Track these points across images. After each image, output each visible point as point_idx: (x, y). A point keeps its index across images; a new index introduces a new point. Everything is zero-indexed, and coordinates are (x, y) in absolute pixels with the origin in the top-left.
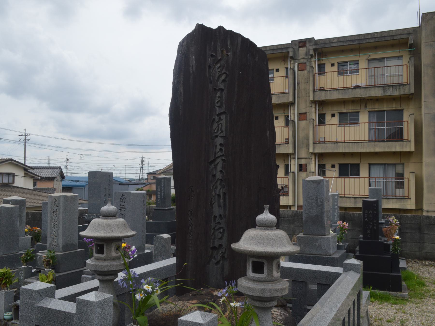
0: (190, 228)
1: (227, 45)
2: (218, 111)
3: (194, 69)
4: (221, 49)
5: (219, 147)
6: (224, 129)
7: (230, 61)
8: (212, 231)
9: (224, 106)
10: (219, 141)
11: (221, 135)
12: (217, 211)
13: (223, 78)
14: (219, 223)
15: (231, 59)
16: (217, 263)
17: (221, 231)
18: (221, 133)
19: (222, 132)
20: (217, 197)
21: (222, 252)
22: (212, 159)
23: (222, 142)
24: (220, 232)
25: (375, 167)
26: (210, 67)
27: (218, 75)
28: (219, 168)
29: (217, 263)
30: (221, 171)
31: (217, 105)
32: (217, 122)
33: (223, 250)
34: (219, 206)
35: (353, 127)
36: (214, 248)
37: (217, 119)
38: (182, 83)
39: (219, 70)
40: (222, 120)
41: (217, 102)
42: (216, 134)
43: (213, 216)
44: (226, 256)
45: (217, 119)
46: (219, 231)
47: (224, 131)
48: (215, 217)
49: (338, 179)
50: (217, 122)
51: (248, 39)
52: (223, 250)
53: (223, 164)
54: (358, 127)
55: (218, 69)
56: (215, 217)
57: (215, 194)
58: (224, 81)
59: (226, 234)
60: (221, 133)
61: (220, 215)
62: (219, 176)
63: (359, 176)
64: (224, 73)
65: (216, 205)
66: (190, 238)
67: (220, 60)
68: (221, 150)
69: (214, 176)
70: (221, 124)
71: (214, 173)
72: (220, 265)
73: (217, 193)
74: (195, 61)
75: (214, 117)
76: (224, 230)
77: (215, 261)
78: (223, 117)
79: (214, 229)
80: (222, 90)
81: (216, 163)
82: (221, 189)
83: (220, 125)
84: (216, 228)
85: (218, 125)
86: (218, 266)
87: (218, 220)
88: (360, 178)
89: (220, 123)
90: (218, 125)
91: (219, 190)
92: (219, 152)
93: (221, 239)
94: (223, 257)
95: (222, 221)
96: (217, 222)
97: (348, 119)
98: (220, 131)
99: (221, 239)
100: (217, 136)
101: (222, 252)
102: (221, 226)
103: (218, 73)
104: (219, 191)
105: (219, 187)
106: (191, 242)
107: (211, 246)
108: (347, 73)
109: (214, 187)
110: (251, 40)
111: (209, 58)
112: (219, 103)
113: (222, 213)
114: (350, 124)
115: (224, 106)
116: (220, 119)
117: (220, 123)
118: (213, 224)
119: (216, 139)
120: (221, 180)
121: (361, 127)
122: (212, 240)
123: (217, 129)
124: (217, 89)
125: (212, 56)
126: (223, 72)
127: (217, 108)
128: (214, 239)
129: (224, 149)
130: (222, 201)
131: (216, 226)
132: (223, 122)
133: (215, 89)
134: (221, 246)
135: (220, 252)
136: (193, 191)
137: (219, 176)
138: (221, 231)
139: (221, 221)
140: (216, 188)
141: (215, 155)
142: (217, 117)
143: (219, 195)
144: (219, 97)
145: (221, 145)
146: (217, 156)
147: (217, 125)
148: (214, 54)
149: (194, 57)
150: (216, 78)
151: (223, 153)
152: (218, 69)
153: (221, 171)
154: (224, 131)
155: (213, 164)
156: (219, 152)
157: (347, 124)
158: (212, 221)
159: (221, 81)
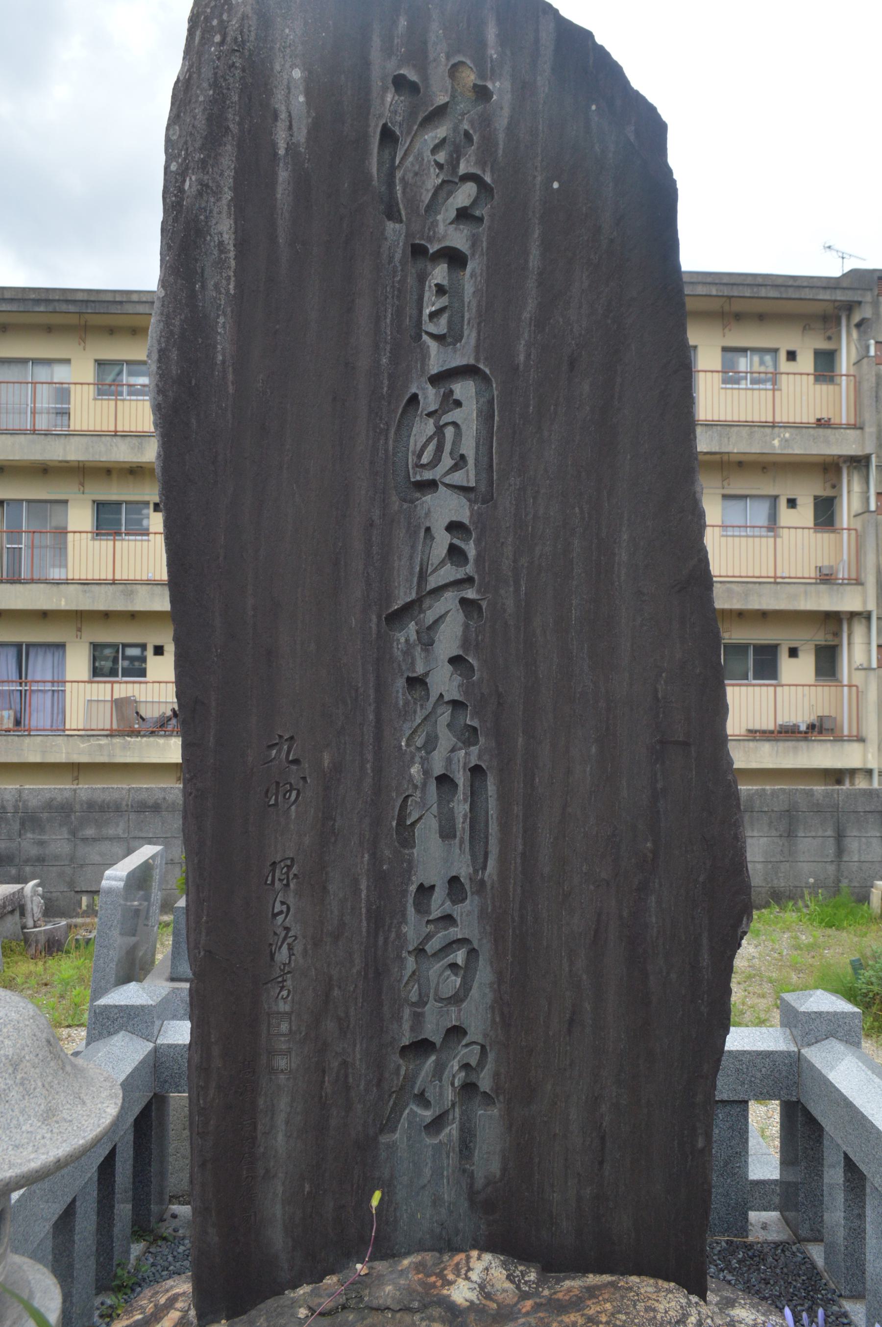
0: (283, 955)
1: (482, 44)
2: (437, 360)
3: (301, 135)
4: (448, 58)
5: (443, 540)
6: (468, 448)
7: (502, 122)
8: (411, 963)
9: (470, 336)
10: (445, 508)
11: (458, 478)
12: (434, 858)
13: (464, 195)
14: (448, 919)
15: (506, 112)
16: (437, 1124)
17: (460, 957)
18: (455, 468)
19: (461, 462)
20: (432, 786)
21: (466, 1066)
22: (404, 595)
23: (464, 517)
24: (453, 966)
25: (41, 652)
26: (388, 136)
27: (434, 179)
28: (448, 641)
29: (437, 1124)
30: (455, 661)
31: (431, 328)
32: (430, 415)
33: (472, 1055)
34: (447, 833)
35: (139, 543)
36: (422, 1047)
37: (430, 398)
38: (228, 195)
39: (441, 157)
40: (458, 404)
41: (433, 315)
42: (428, 475)
43: (413, 888)
44: (485, 1082)
45: (430, 398)
46: (450, 959)
47: (471, 461)
48: (425, 891)
49: (88, 686)
50: (430, 415)
51: (588, 35)
52: (472, 1055)
53: (466, 627)
54: (145, 544)
55: (435, 150)
56: (425, 891)
57: (426, 773)
58: (463, 215)
59: (484, 974)
60: (455, 468)
61: (454, 881)
62: (444, 682)
63: (144, 675)
64: (468, 177)
65: (427, 833)
66: (283, 1007)
67: (440, 112)
68: (455, 553)
69: (417, 683)
70: (455, 424)
71: (420, 670)
72: (452, 1130)
73: (438, 770)
74: (308, 93)
75: (414, 390)
76: (473, 953)
77: (428, 1115)
78: (464, 389)
79: (420, 951)
80: (455, 259)
81: (430, 617)
82: (453, 750)
83: (449, 432)
84: (432, 946)
85: (440, 430)
86: (443, 1136)
87: (439, 904)
88: (146, 683)
89: (446, 418)
90: (440, 430)
91: (449, 754)
92: (442, 563)
93: (457, 999)
94: (469, 1088)
95: (467, 911)
96: (435, 914)
97: (120, 520)
98: (447, 462)
99: (457, 999)
100: (431, 485)
101: (466, 1066)
102: (456, 932)
103: (434, 170)
104: (449, 761)
105: (446, 739)
106: (284, 1027)
107: (406, 1041)
108: (121, 394)
109: (420, 741)
110: (599, 40)
111: (385, 89)
112: (444, 320)
113: (463, 869)
114: (126, 534)
115: (470, 336)
116: (451, 402)
117: (446, 418)
118: (413, 928)
119: (428, 498)
120: (456, 704)
121: (151, 543)
122: (407, 1012)
123: (431, 447)
124: (433, 248)
125: (400, 83)
126: (463, 169)
127: (433, 345)
128: (422, 1002)
129: (471, 550)
130: (461, 808)
131: (429, 937)
132: (468, 416)
133: (418, 251)
134: (456, 1032)
135: (456, 1068)
136: (296, 762)
137: (444, 682)
138: (460, 957)
139: (457, 911)
140: (431, 744)
141: (423, 577)
142: (431, 391)
143: (445, 781)
144: (440, 290)
145: (454, 527)
146: (433, 582)
147: (430, 427)
148: (413, 76)
149: (297, 74)
150: (427, 197)
151: (470, 569)
152: (435, 150)
153: (455, 661)
154: (471, 461)
155: (412, 626)
156: (442, 563)
157: (120, 534)
158: (411, 910)
159: (453, 214)
